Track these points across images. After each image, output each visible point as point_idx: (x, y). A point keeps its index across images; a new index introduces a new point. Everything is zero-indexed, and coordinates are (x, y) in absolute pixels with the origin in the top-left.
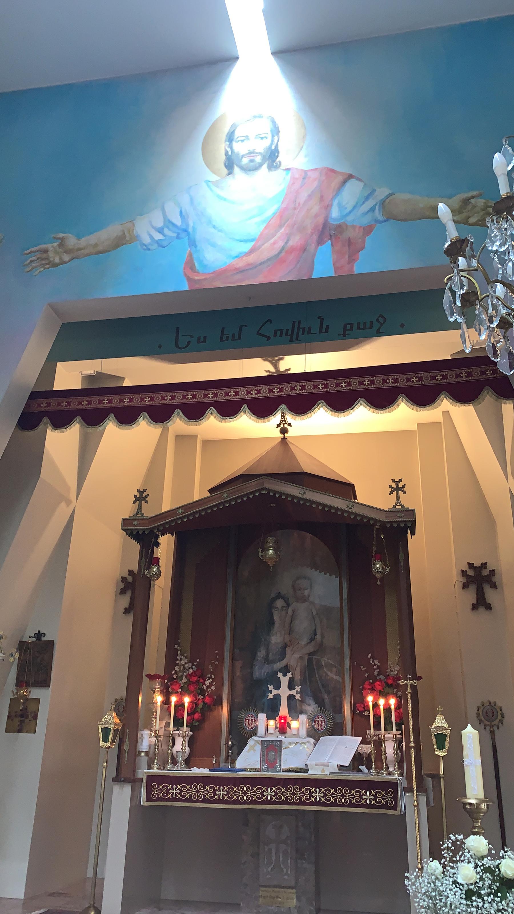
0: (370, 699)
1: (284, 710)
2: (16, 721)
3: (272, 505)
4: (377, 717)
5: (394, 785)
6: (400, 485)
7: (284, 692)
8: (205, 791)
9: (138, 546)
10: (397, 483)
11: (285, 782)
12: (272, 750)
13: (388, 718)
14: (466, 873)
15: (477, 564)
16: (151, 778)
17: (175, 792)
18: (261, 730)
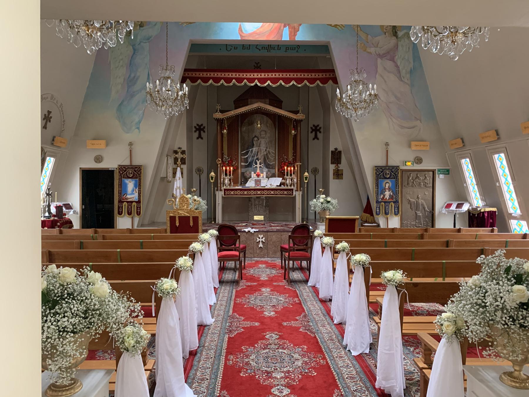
0: (286, 168)
1: (258, 171)
2: (340, 173)
3: (132, 38)
4: (287, 173)
5: (292, 190)
6: (259, 65)
7: (258, 165)
8: (240, 192)
9: (525, 222)
10: (257, 64)
11: (263, 190)
12: (258, 182)
13: (230, 172)
14: (322, 200)
15: (316, 125)
16: (225, 190)
17: (232, 193)
18: (252, 177)
